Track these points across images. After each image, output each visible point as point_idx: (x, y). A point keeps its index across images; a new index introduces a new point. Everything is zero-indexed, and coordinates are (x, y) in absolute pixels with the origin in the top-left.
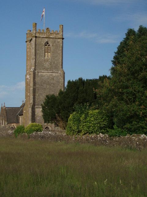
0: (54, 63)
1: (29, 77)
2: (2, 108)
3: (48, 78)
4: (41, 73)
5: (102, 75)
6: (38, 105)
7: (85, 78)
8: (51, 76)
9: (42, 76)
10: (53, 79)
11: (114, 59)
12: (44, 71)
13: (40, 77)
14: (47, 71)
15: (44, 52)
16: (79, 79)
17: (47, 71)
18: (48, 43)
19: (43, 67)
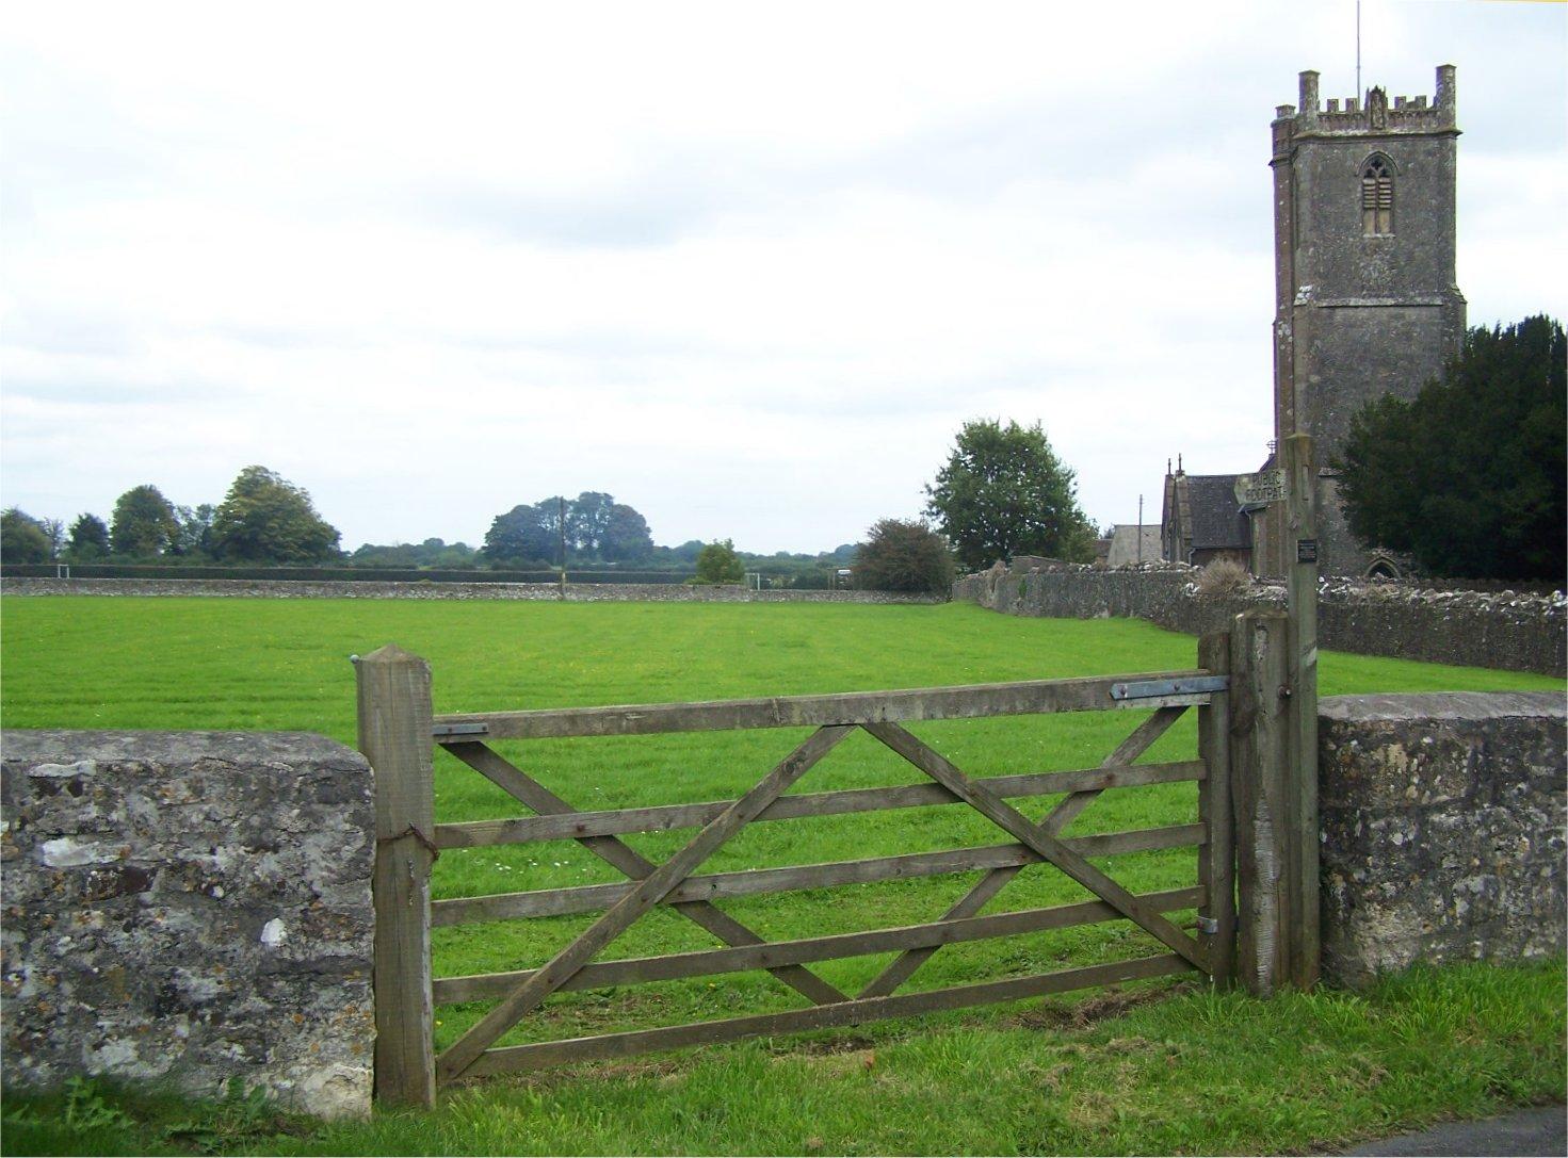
0: (1410, 257)
1: (1288, 332)
2: (1169, 477)
3: (1381, 332)
4: (1346, 311)
5: (427, 538)
6: (1300, 381)
7: (488, 528)
8: (1394, 324)
9: (1351, 326)
10: (1408, 337)
11: (941, 503)
12: (1361, 302)
13: (1341, 331)
14: (1374, 302)
15: (1358, 208)
16: (1481, 329)
17: (1374, 302)
18: (1003, 1012)
19: (1356, 280)
